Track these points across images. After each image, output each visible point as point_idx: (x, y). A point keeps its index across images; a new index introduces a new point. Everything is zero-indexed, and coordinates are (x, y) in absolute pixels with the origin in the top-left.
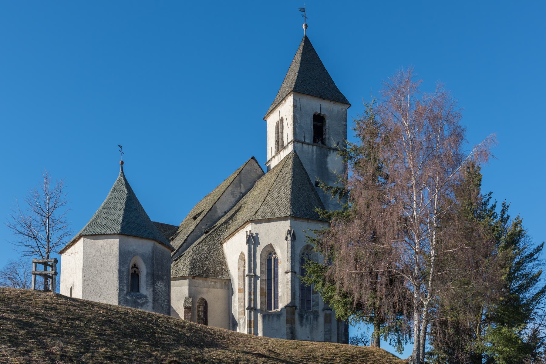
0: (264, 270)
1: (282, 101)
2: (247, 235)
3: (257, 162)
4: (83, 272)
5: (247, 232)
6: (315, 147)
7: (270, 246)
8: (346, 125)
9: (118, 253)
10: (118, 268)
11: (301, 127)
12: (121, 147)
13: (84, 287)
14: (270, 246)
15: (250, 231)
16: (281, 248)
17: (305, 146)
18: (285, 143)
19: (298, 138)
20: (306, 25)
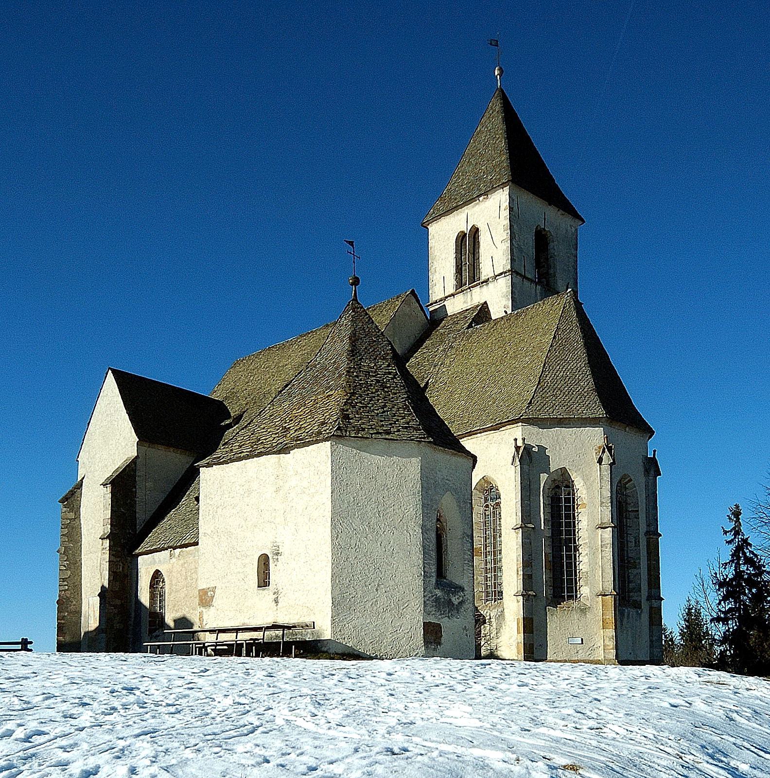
0: (429, 525)
2: (517, 448)
3: (418, 301)
4: (334, 526)
5: (516, 440)
6: (539, 287)
7: (564, 472)
11: (520, 250)
12: (351, 243)
13: (335, 564)
14: (564, 472)
15: (524, 439)
16: (586, 479)
17: (526, 283)
18: (486, 270)
19: (516, 268)
20: (500, 69)
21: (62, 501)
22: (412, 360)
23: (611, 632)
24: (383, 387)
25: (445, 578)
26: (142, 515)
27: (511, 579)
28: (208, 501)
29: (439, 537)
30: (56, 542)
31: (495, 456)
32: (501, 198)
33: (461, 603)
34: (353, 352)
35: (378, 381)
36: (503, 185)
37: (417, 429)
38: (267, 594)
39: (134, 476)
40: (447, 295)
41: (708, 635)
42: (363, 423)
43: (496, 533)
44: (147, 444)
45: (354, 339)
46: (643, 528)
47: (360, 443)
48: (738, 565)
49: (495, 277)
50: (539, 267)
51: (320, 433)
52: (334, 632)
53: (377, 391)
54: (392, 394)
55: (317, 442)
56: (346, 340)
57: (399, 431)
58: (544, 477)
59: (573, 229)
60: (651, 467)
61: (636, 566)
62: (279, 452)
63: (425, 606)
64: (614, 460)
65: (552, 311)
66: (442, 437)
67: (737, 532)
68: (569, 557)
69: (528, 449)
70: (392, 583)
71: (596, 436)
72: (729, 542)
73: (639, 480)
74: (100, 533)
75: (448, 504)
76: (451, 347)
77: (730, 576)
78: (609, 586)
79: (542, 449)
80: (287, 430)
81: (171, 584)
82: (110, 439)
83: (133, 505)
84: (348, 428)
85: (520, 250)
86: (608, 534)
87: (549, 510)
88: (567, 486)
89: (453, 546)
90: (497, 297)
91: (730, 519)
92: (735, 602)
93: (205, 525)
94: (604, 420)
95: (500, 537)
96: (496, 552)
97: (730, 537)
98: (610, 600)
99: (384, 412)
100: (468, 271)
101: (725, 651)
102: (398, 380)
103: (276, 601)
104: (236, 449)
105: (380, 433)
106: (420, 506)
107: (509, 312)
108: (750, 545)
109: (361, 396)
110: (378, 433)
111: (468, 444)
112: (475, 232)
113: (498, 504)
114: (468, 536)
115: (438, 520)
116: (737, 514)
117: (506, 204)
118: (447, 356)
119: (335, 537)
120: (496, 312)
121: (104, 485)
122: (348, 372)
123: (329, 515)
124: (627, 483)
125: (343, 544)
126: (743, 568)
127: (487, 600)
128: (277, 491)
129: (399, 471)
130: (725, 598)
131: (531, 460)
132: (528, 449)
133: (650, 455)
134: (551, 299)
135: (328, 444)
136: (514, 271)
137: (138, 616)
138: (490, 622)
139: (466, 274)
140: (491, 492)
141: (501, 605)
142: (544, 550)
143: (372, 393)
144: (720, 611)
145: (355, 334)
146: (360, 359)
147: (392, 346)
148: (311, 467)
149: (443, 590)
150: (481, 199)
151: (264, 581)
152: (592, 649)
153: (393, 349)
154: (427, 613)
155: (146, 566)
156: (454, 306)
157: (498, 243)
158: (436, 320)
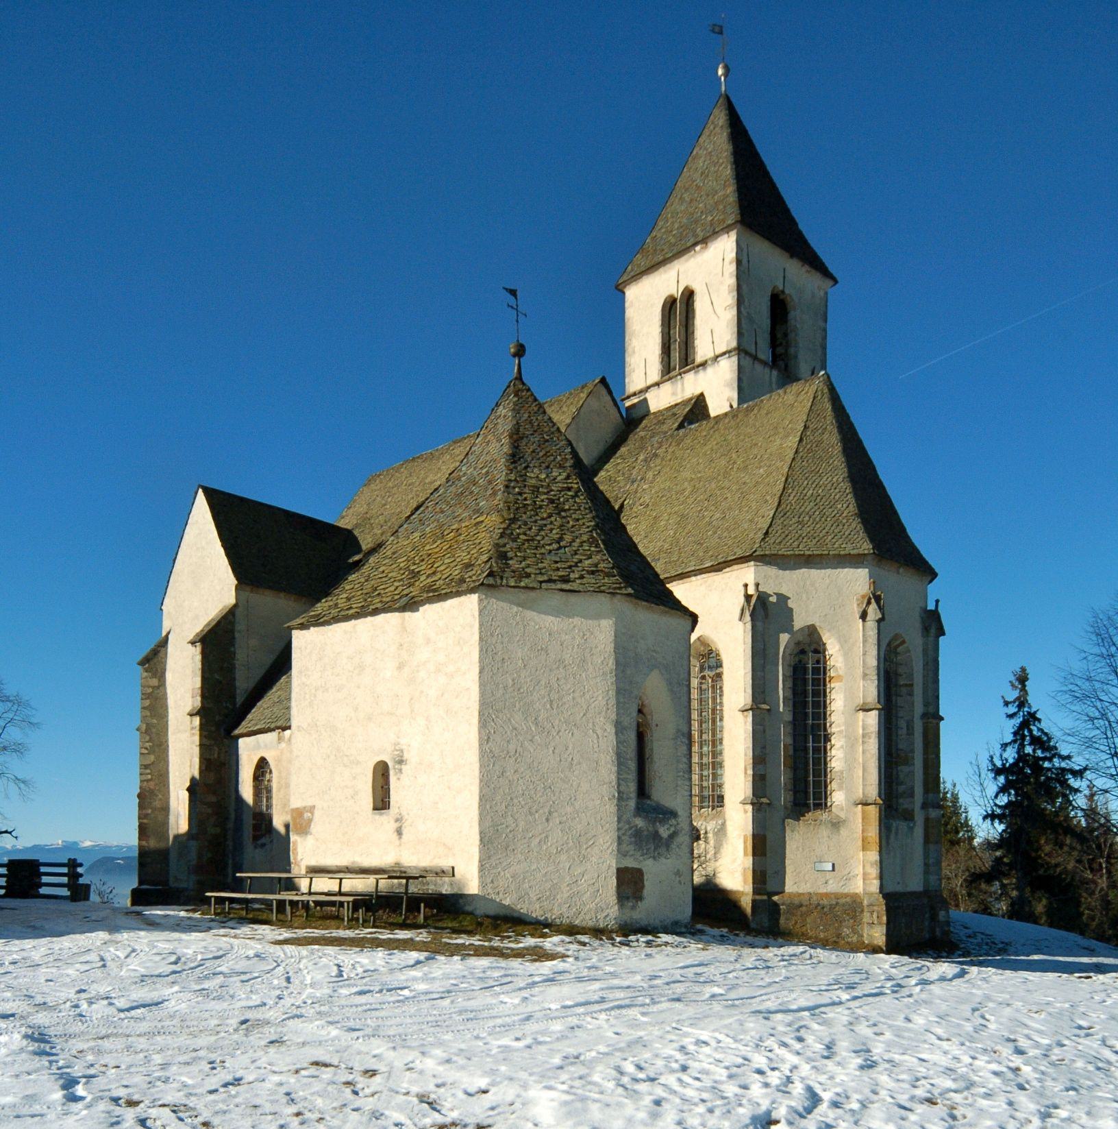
1: (695, 244)
2: (748, 597)
3: (610, 392)
4: (483, 724)
5: (746, 586)
6: (775, 373)
8: (825, 330)
9: (611, 663)
10: (614, 717)
11: (751, 320)
12: (513, 293)
15: (757, 585)
16: (843, 641)
18: (703, 349)
20: (727, 69)
21: (142, 663)
22: (602, 473)
23: (874, 856)
24: (559, 510)
25: (649, 797)
26: (243, 683)
27: (737, 779)
28: (304, 679)
29: (641, 737)
30: (134, 717)
31: (717, 605)
32: (725, 248)
33: (673, 836)
34: (515, 457)
35: (552, 501)
36: (727, 229)
37: (608, 575)
38: (386, 821)
39: (232, 631)
40: (649, 383)
41: (967, 825)
42: (528, 566)
43: (716, 715)
44: (248, 588)
45: (516, 437)
46: (919, 709)
47: (523, 595)
48: (1022, 746)
49: (716, 358)
50: (775, 343)
51: (462, 581)
52: (483, 884)
53: (550, 516)
54: (570, 525)
55: (458, 594)
56: (506, 440)
57: (582, 577)
58: (784, 638)
59: (822, 293)
60: (932, 623)
61: (908, 761)
62: (403, 609)
63: (619, 844)
64: (883, 614)
65: (795, 403)
66: (646, 586)
67: (1022, 703)
68: (817, 750)
69: (762, 599)
70: (569, 809)
71: (857, 580)
72: (1011, 716)
73: (915, 641)
74: (188, 709)
75: (655, 689)
76: (656, 455)
77: (1011, 761)
78: (873, 792)
79: (783, 599)
80: (415, 575)
81: (280, 777)
82: (202, 581)
83: (232, 669)
84: (502, 574)
85: (751, 320)
86: (873, 719)
87: (790, 684)
88: (816, 651)
89: (662, 750)
90: (717, 386)
91: (1013, 685)
92: (1016, 795)
93: (299, 714)
94: (869, 558)
95: (721, 720)
96: (716, 742)
97: (1012, 709)
98: (873, 811)
99: (560, 548)
100: (678, 351)
101: (1001, 858)
102: (581, 499)
103: (399, 832)
104: (342, 602)
105: (554, 581)
106: (612, 693)
107: (735, 406)
108: (1039, 720)
109: (526, 524)
110: (550, 581)
111: (680, 590)
112: (689, 295)
113: (719, 676)
114: (683, 735)
115: (640, 711)
116: (1022, 679)
117: (732, 255)
118: (649, 468)
119: (486, 739)
120: (719, 404)
121: (193, 643)
122: (507, 487)
123: (475, 707)
124: (898, 646)
125: (497, 752)
126: (1029, 750)
127: (702, 807)
128: (401, 667)
129: (584, 637)
130: (1003, 790)
131: (767, 616)
132: (762, 599)
133: (931, 607)
134: (795, 387)
135: (474, 597)
136: (742, 350)
137: (239, 820)
138: (706, 838)
139: (676, 356)
140: (711, 660)
141: (721, 815)
142: (783, 737)
143: (543, 519)
144: (996, 805)
145: (518, 431)
146: (526, 468)
147: (572, 448)
148: (451, 629)
149: (646, 818)
150: (698, 248)
151: (382, 802)
152: (849, 878)
153: (574, 453)
154: (622, 854)
155: (249, 750)
156: (659, 400)
157: (719, 310)
158: (633, 419)
